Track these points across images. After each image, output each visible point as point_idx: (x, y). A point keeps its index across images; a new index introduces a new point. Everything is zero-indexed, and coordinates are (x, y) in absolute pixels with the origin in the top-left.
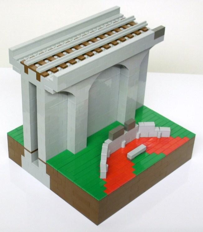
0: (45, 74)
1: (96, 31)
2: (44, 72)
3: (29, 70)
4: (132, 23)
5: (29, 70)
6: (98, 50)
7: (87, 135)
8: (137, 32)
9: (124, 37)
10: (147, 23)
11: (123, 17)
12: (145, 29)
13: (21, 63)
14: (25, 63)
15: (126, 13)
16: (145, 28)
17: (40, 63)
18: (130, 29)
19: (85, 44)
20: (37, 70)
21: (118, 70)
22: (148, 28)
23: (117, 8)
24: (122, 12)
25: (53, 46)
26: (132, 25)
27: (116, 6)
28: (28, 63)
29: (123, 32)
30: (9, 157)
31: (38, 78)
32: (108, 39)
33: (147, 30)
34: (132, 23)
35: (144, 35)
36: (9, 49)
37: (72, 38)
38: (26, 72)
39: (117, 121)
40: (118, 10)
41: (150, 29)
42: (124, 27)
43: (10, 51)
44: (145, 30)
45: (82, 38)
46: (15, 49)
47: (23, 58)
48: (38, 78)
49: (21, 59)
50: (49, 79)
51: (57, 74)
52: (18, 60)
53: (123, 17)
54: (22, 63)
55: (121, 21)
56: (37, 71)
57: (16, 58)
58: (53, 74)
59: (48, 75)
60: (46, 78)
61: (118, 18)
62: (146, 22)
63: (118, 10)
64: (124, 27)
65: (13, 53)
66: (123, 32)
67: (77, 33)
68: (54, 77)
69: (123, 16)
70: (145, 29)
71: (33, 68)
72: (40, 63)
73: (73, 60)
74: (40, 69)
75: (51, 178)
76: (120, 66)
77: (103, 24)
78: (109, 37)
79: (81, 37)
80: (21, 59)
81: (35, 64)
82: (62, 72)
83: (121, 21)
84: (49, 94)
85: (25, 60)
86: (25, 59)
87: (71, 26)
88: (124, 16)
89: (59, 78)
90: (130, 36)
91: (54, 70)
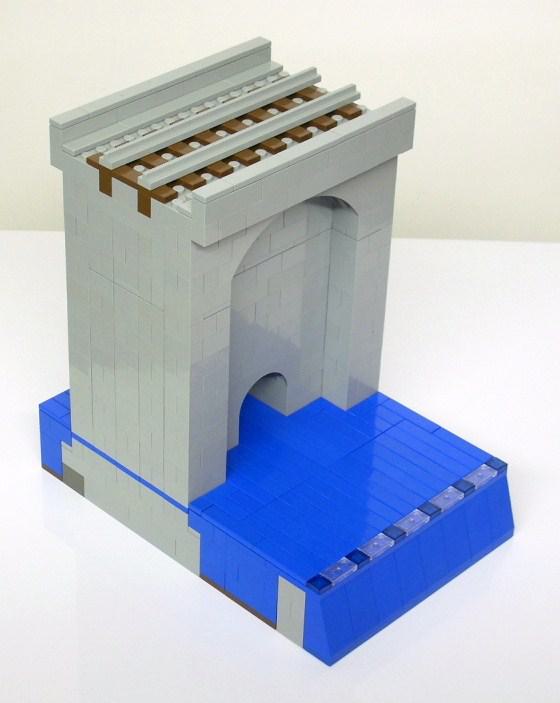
0: (166, 193)
1: (187, 120)
2: (160, 189)
3: (115, 182)
4: (307, 93)
5: (115, 182)
6: (273, 145)
7: (228, 445)
8: (324, 123)
9: (306, 125)
10: (358, 89)
11: (281, 74)
12: (350, 112)
13: (90, 161)
14: (102, 161)
15: (290, 59)
16: (351, 106)
17: (149, 161)
18: (300, 112)
19: (203, 138)
20: (141, 181)
21: (323, 217)
22: (363, 109)
23: (261, 44)
24: (277, 57)
25: (210, 101)
26: (307, 99)
27: (260, 38)
28: (110, 162)
29: (276, 122)
30: (45, 466)
31: (144, 208)
32: (199, 156)
33: (359, 113)
34: (307, 93)
35: (345, 128)
36: (51, 121)
37: (136, 131)
38: (106, 188)
39: (321, 399)
40: (263, 51)
41: (366, 110)
42: (281, 105)
43: (53, 125)
44: (350, 112)
45: (168, 131)
46: (84, 114)
47: (93, 147)
48: (144, 208)
49: (87, 150)
50: (178, 208)
51: (203, 192)
52: (79, 154)
53: (281, 74)
54: (92, 162)
55: (248, 95)
56: (139, 183)
57: (73, 147)
58: (189, 194)
59: (175, 195)
60: (167, 205)
61: (264, 78)
62: (353, 88)
63: (263, 51)
64: (281, 105)
65: (62, 132)
66: (276, 122)
67: (124, 126)
68: (197, 199)
69: (281, 68)
70: (350, 112)
71: (127, 176)
72: (149, 161)
73: (326, 118)
74: (150, 178)
75: (203, 540)
76: (331, 203)
77: (239, 88)
78: (177, 159)
79: (244, 96)
80: (273, 75)
81: (131, 164)
82: (214, 187)
83: (248, 95)
84: (199, 246)
85: (101, 154)
86: (100, 149)
87: (229, 56)
88: (284, 69)
89: (211, 199)
90: (299, 134)
91: (192, 181)
